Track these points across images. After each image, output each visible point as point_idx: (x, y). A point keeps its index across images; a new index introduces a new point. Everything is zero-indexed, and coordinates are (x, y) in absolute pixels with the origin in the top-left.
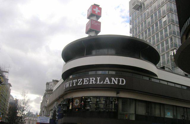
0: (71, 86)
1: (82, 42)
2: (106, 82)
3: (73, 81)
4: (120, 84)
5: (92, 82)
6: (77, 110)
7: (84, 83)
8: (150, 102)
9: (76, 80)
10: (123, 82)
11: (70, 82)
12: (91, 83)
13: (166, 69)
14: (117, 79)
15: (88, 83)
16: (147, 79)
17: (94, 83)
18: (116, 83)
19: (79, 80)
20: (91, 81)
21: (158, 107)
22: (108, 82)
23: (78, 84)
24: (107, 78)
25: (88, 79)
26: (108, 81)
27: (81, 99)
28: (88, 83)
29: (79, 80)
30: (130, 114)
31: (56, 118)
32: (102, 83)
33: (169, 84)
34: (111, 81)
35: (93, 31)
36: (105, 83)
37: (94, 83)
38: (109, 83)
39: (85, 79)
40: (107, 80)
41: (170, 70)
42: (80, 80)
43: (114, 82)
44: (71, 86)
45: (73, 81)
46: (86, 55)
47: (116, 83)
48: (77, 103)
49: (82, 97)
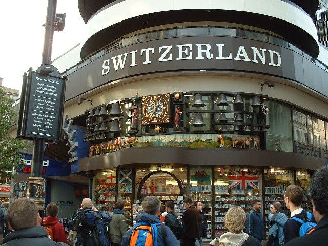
0: (133, 64)
3: (142, 51)
5: (204, 54)
7: (181, 58)
9: (152, 49)
10: (276, 61)
12: (200, 57)
14: (264, 50)
15: (190, 57)
19: (160, 48)
20: (200, 51)
22: (244, 58)
23: (161, 59)
24: (242, 48)
25: (190, 46)
26: (245, 54)
28: (190, 57)
31: (70, 156)
36: (237, 58)
37: (208, 56)
38: (247, 59)
39: (181, 46)
40: (242, 53)
42: (163, 50)
43: (258, 58)
44: (133, 64)
45: (142, 51)
49: (172, 95)
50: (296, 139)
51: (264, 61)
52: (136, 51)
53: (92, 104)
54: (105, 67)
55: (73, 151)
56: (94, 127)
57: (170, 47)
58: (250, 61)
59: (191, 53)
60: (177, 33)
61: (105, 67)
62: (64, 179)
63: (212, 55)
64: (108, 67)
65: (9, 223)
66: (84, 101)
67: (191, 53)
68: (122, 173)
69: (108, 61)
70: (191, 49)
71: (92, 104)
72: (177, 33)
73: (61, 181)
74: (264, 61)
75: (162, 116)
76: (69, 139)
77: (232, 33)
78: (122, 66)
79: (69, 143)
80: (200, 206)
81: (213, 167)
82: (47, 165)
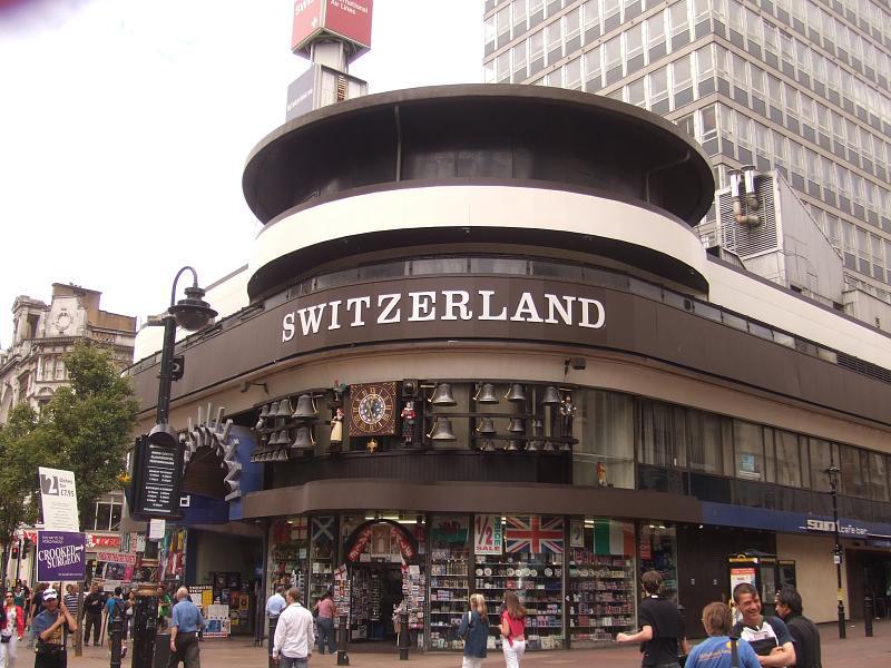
0: (335, 325)
1: (397, 109)
2: (522, 315)
3: (350, 302)
4: (585, 323)
5: (456, 310)
6: (373, 444)
7: (415, 317)
8: (685, 409)
9: (367, 299)
10: (593, 317)
11: (328, 310)
12: (449, 316)
13: (723, 257)
14: (570, 299)
15: (432, 317)
16: (679, 302)
17: (464, 316)
18: (568, 319)
19: (381, 298)
20: (450, 304)
21: (709, 426)
22: (529, 315)
23: (381, 319)
24: (527, 297)
25: (433, 295)
26: (532, 309)
27: (402, 393)
28: (432, 317)
29: (381, 298)
30: (612, 463)
31: (228, 489)
32: (503, 317)
33: (754, 329)
34: (543, 308)
35: (335, 41)
36: (517, 318)
37: (464, 316)
38: (535, 318)
39: (416, 296)
40: (526, 306)
41: (737, 264)
42: (386, 302)
43: (557, 315)
44: (335, 325)
45: (350, 302)
46: (401, 179)
47: (568, 319)
48: (374, 413)
49: (400, 384)
50: (640, 460)
51: (568, 319)
52: (340, 302)
53: (267, 391)
54: (287, 326)
55: (233, 479)
56: (269, 436)
57: (397, 297)
58: (541, 320)
59: (434, 309)
60: (469, 266)
61: (287, 326)
62: (220, 528)
63: (471, 313)
64: (291, 327)
65: (93, 627)
66: (252, 387)
67: (434, 309)
68: (317, 522)
69: (292, 316)
70: (434, 301)
71: (267, 391)
72: (469, 266)
73: (214, 533)
74: (568, 319)
75: (382, 421)
76: (227, 456)
77: (516, 268)
78: (315, 330)
79: (225, 463)
80: (494, 440)
81: (472, 515)
82: (188, 505)
